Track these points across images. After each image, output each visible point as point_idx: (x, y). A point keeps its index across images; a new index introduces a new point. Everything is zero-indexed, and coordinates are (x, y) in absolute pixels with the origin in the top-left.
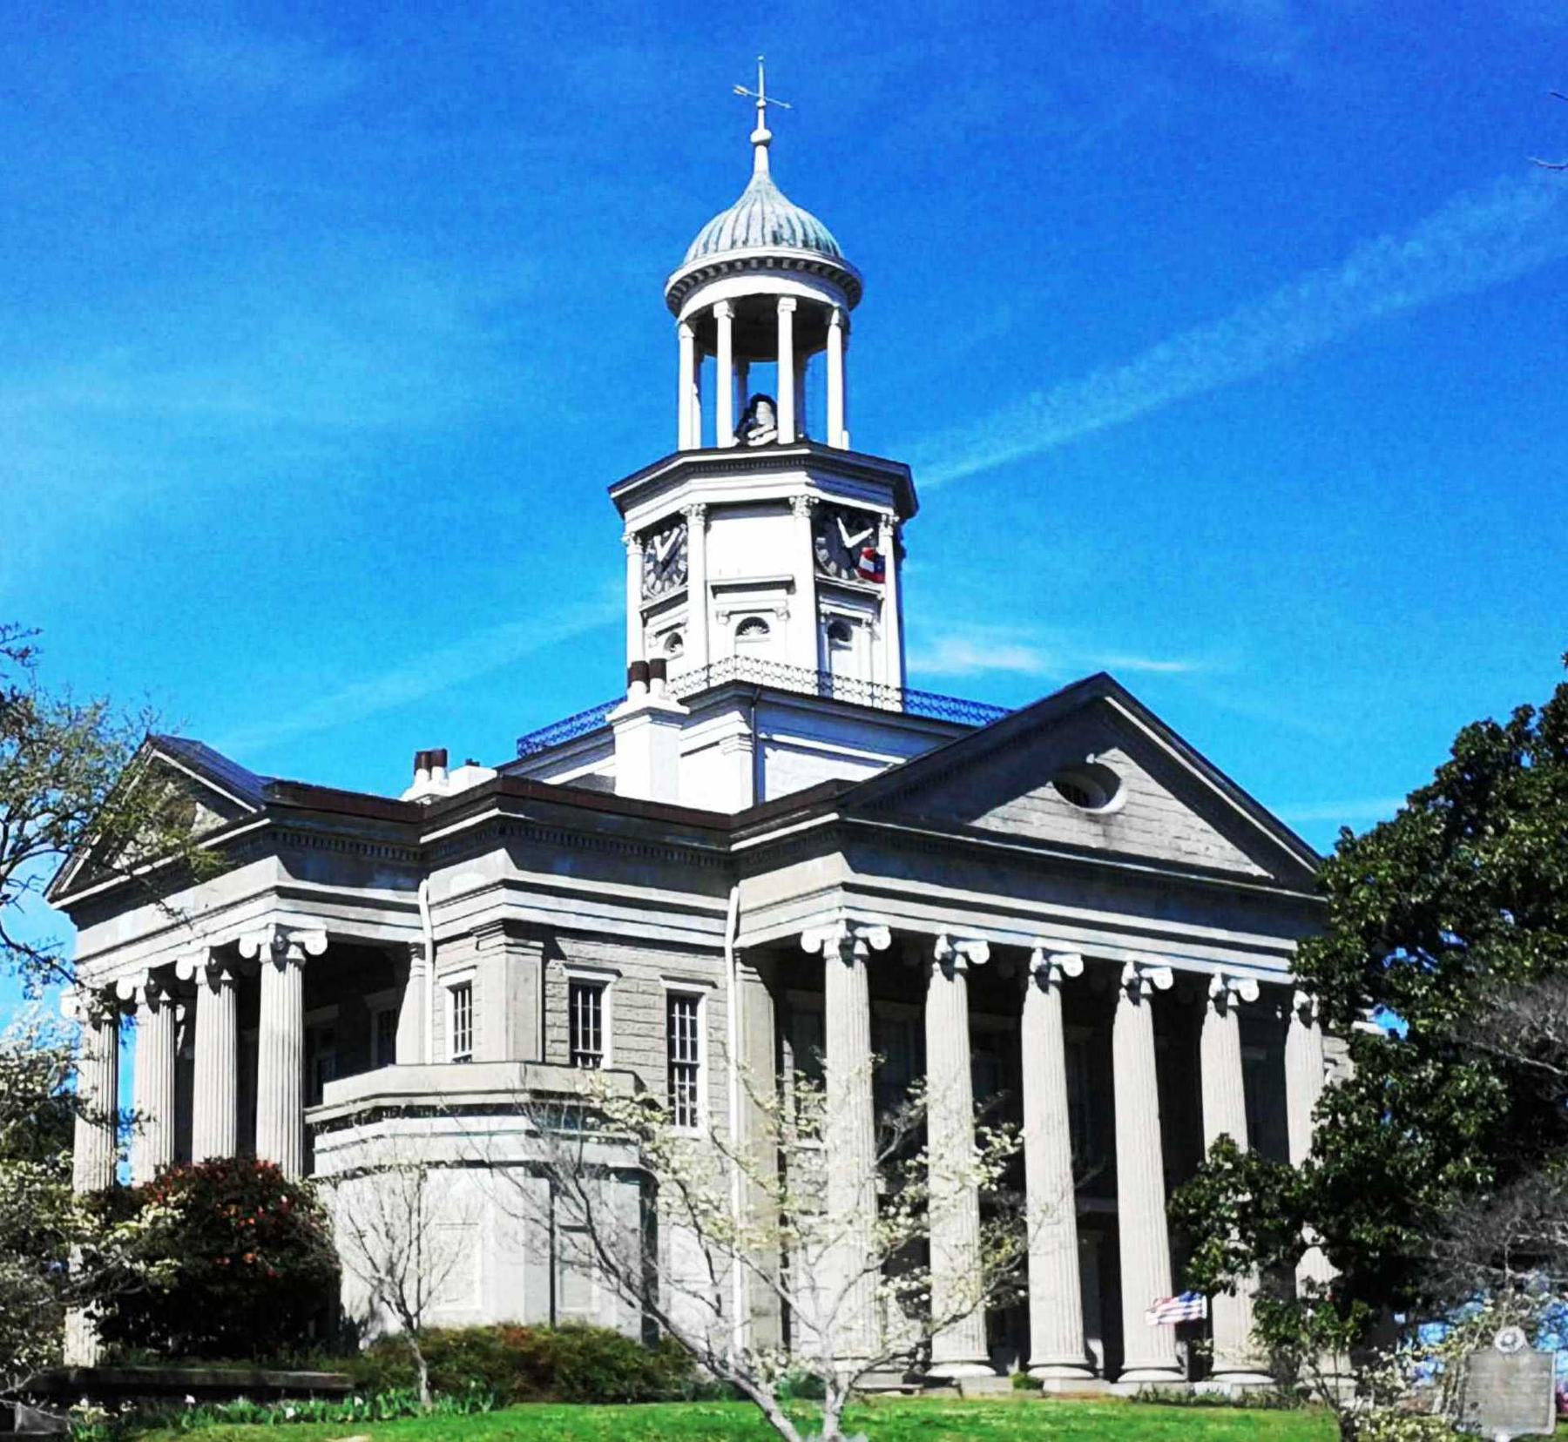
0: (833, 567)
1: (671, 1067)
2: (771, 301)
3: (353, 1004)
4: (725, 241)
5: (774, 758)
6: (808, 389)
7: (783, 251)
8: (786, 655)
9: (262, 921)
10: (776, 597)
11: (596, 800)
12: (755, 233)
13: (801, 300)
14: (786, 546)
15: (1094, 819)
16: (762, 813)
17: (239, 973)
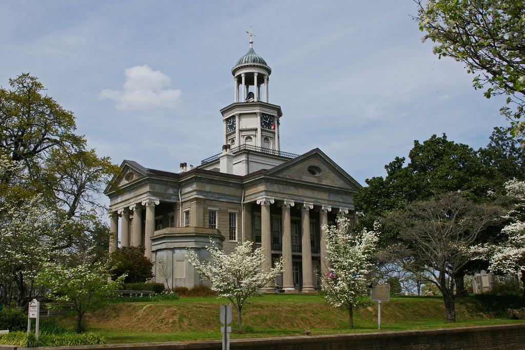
0: (265, 126)
1: (230, 228)
2: (252, 74)
3: (165, 213)
4: (244, 62)
5: (251, 164)
6: (261, 91)
7: (255, 64)
8: (256, 143)
9: (146, 198)
10: (253, 133)
11: (217, 173)
12: (250, 60)
13: (258, 73)
14: (255, 122)
15: (316, 177)
16: (248, 176)
17: (142, 210)
